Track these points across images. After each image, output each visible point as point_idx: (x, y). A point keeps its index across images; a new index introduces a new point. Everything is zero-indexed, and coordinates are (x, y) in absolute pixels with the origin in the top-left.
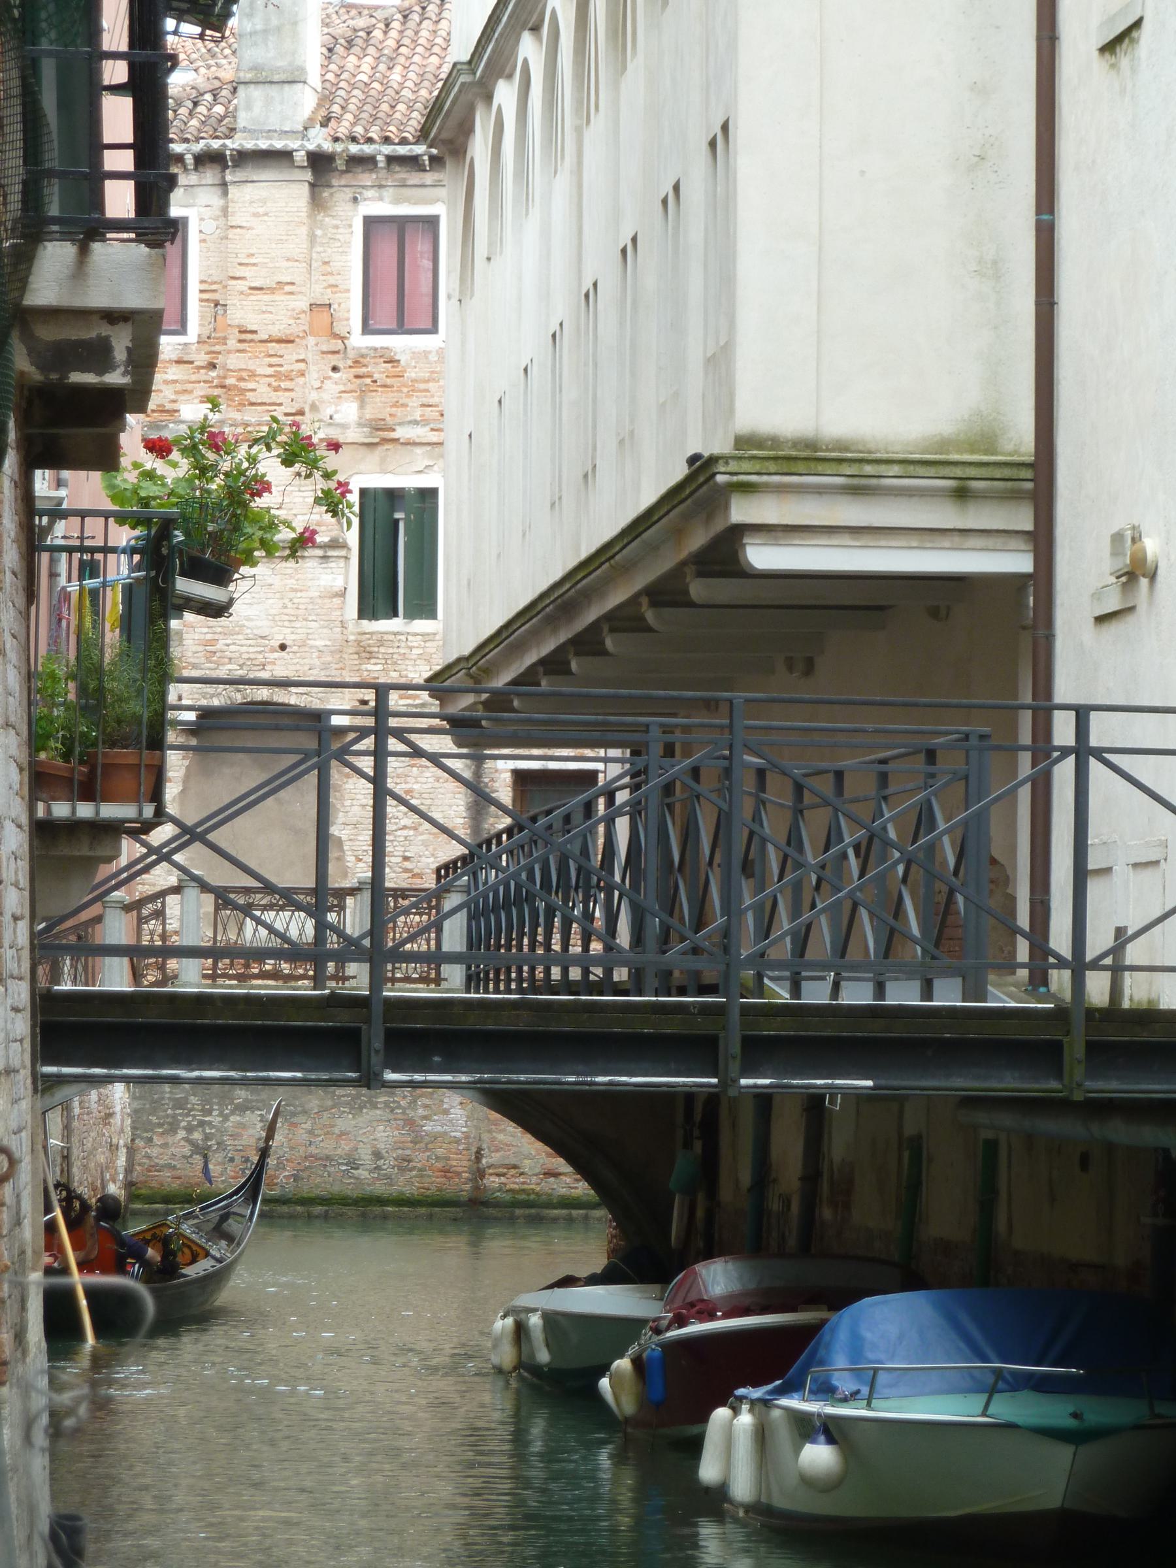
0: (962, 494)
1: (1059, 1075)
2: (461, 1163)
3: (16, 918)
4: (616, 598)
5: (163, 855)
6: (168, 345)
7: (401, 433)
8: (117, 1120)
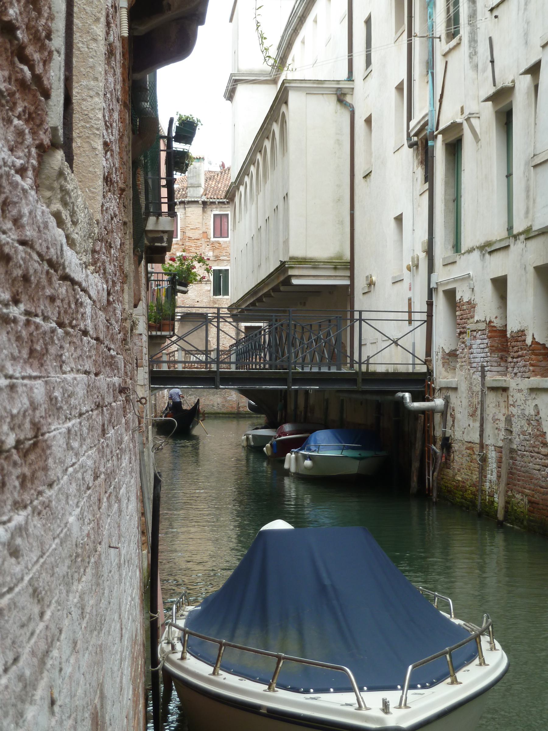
0: (335, 268)
1: (356, 386)
2: (235, 406)
3: (145, 354)
4: (265, 290)
5: (174, 342)
6: (174, 240)
7: (221, 258)
8: (165, 397)
